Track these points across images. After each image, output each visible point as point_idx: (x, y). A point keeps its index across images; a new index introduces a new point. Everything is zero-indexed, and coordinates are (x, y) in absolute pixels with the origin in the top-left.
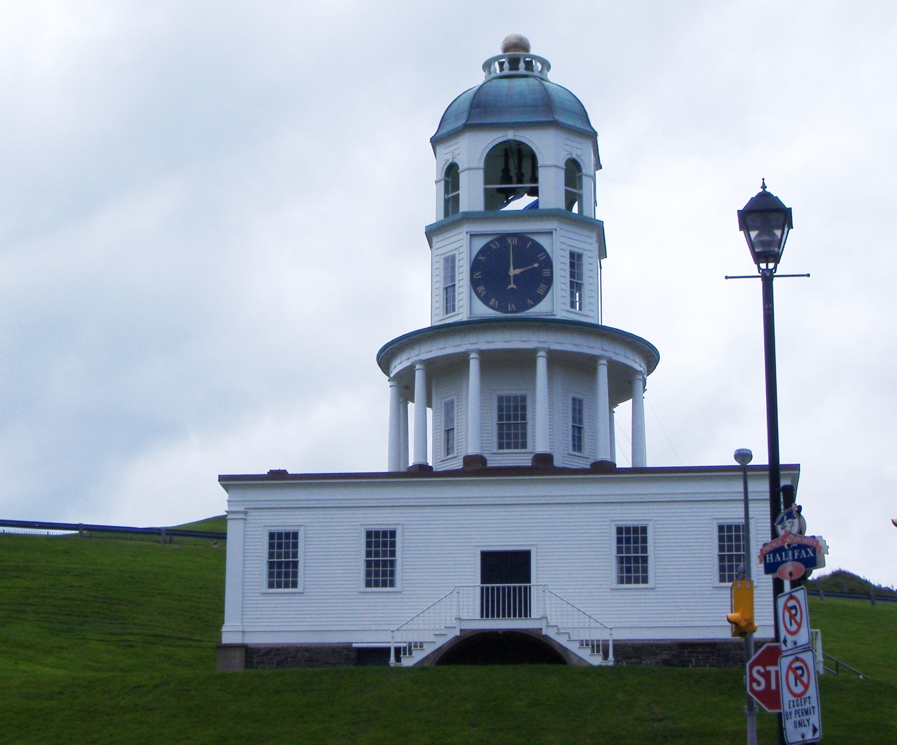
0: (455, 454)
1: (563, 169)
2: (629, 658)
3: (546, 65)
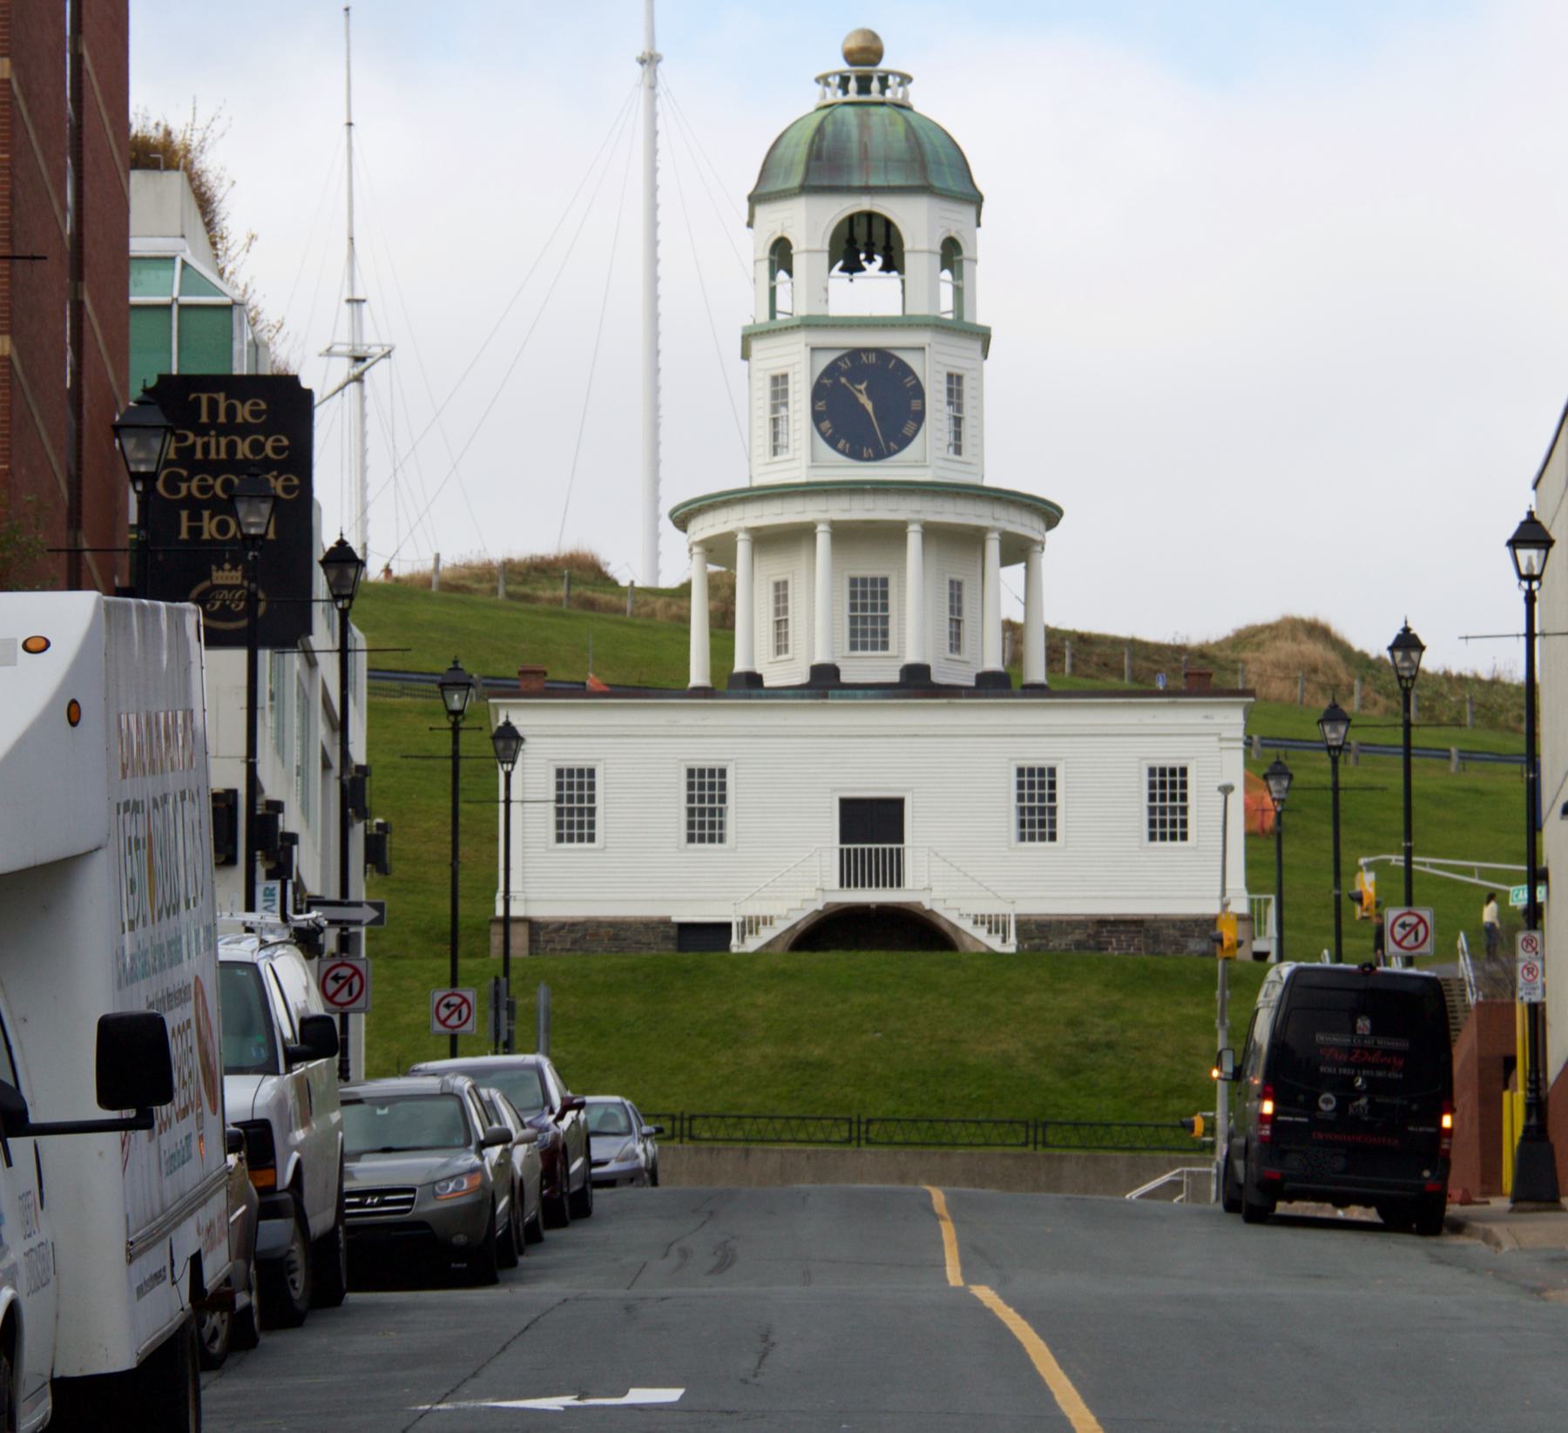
1: (935, 253)
3: (905, 79)
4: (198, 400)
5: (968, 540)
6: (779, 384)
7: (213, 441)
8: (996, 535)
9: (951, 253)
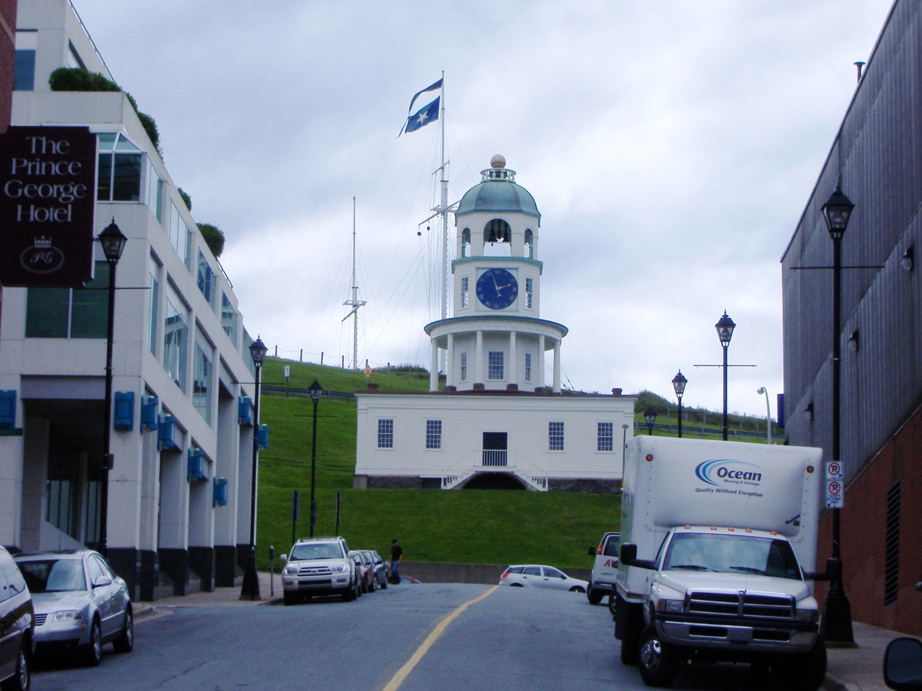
0: (466, 381)
2: (554, 486)
3: (514, 173)
4: (31, 141)
5: (532, 339)
6: (465, 281)
7: (38, 164)
8: (543, 337)
9: (529, 235)
